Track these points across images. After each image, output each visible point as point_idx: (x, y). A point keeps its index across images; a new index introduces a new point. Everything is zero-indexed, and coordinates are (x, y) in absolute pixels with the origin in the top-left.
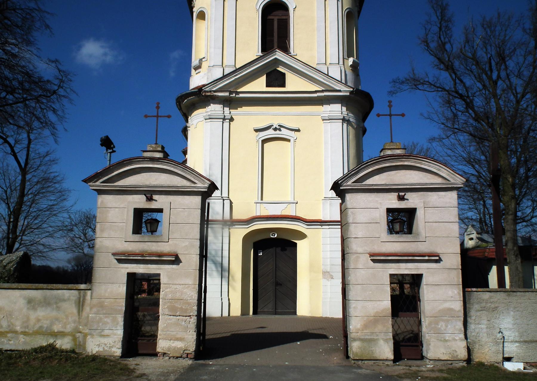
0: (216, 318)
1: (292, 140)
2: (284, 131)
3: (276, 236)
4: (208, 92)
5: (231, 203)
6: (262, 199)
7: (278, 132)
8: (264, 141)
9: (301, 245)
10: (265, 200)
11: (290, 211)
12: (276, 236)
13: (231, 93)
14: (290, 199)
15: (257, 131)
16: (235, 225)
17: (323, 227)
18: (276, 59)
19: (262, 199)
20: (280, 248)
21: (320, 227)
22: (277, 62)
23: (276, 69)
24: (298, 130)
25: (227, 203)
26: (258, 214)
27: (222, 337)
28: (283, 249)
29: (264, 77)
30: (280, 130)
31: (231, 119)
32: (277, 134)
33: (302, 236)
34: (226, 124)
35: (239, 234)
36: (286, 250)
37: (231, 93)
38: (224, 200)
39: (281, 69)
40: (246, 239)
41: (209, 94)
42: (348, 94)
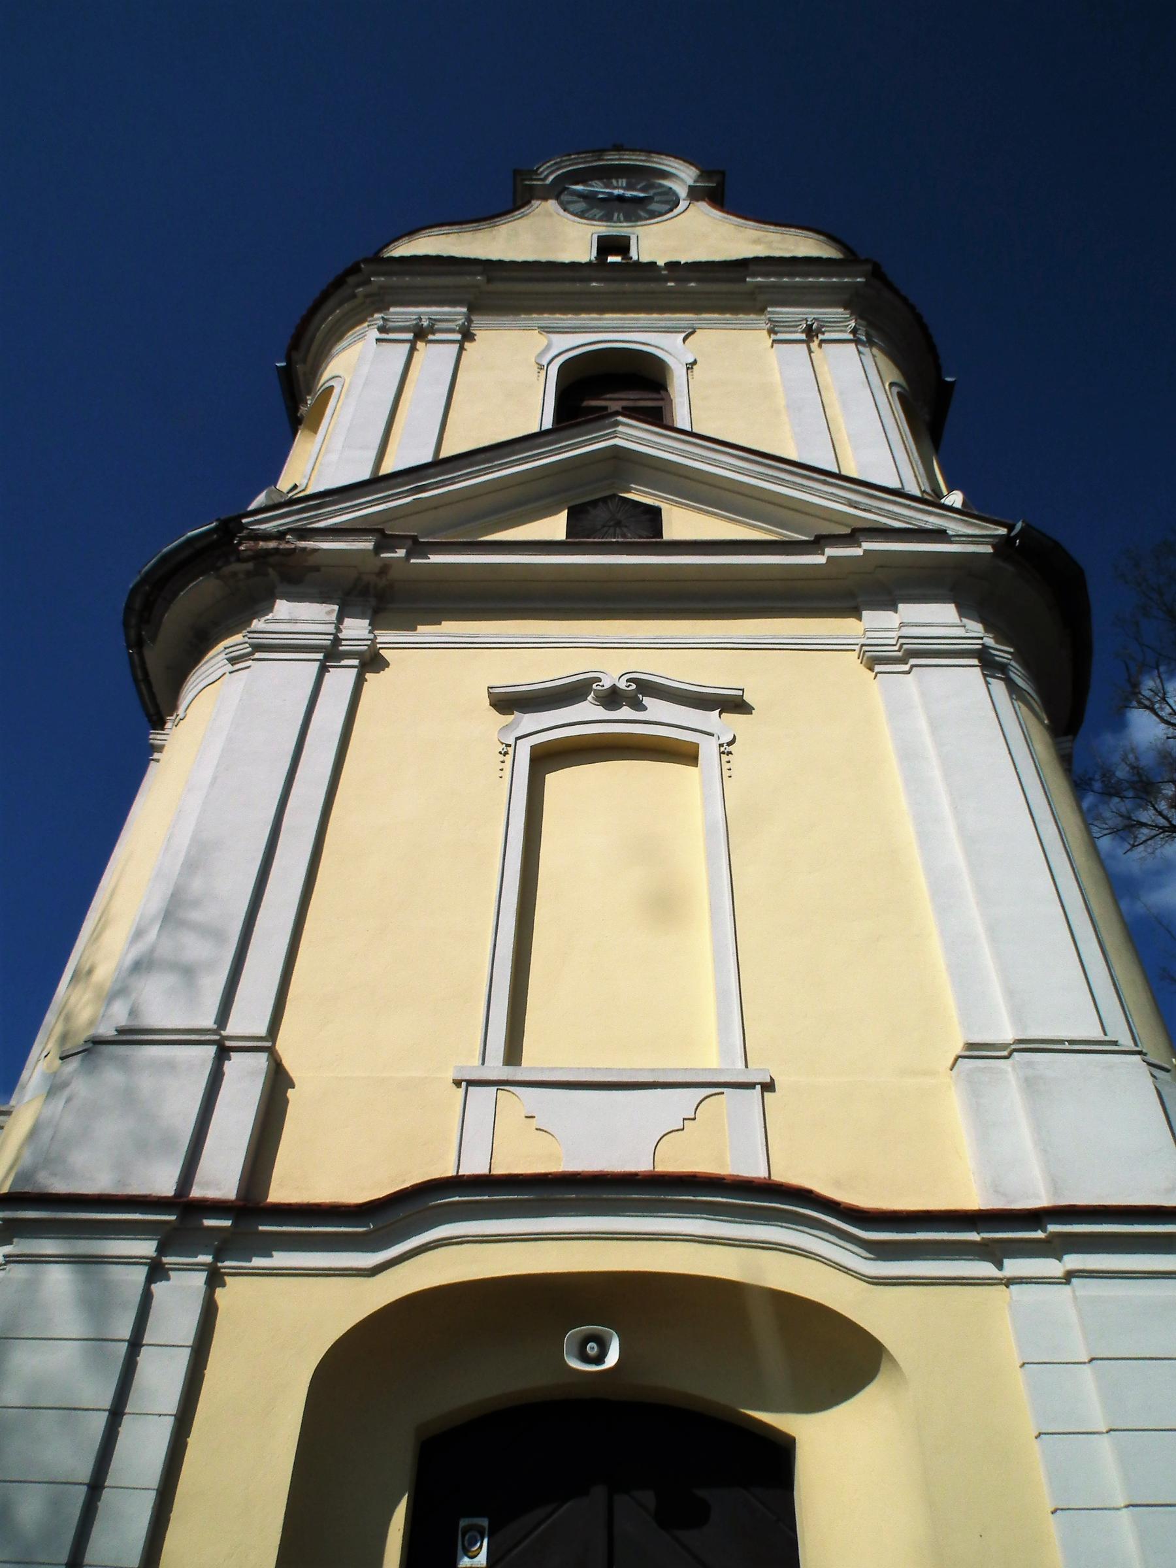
0: (1071, 1253)
1: (708, 750)
2: (656, 708)
3: (612, 1358)
4: (267, 537)
5: (278, 1083)
6: (513, 1054)
7: (626, 712)
8: (549, 758)
9: (842, 1460)
10: (538, 1056)
11: (724, 1146)
12: (612, 1358)
13: (385, 541)
14: (711, 1057)
15: (508, 703)
16: (269, 1244)
17: (1014, 1267)
18: (615, 447)
19: (513, 1054)
20: (648, 1497)
21: (985, 1269)
22: (623, 463)
23: (614, 496)
24: (736, 705)
25: (245, 1079)
26: (475, 1166)
27: (958, 1231)
28: (681, 1514)
29: (563, 515)
30: (638, 706)
31: (372, 662)
32: (621, 722)
33: (840, 1360)
34: (341, 679)
35: (288, 1322)
36: (698, 1516)
37: (385, 541)
38: (223, 1052)
39: (639, 495)
40: (349, 1376)
41: (272, 545)
42: (989, 549)
